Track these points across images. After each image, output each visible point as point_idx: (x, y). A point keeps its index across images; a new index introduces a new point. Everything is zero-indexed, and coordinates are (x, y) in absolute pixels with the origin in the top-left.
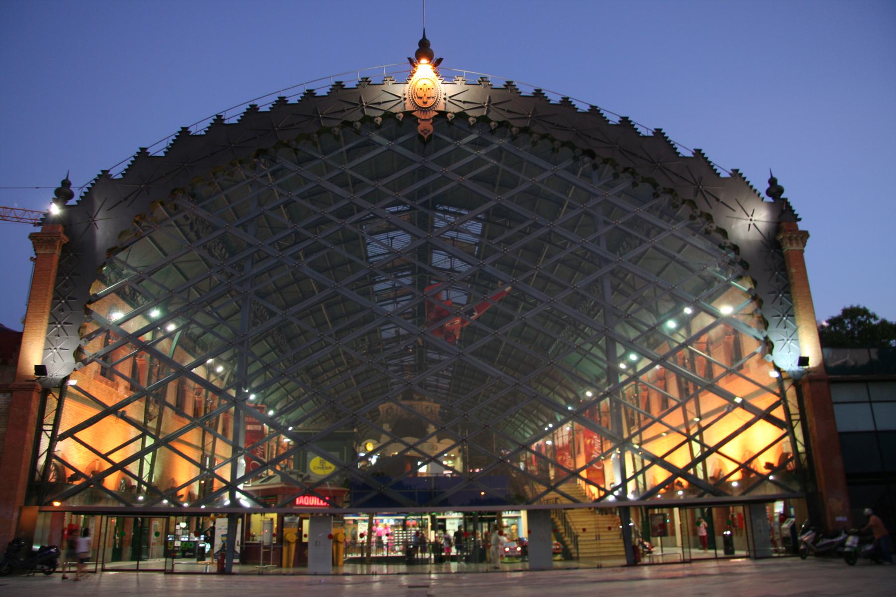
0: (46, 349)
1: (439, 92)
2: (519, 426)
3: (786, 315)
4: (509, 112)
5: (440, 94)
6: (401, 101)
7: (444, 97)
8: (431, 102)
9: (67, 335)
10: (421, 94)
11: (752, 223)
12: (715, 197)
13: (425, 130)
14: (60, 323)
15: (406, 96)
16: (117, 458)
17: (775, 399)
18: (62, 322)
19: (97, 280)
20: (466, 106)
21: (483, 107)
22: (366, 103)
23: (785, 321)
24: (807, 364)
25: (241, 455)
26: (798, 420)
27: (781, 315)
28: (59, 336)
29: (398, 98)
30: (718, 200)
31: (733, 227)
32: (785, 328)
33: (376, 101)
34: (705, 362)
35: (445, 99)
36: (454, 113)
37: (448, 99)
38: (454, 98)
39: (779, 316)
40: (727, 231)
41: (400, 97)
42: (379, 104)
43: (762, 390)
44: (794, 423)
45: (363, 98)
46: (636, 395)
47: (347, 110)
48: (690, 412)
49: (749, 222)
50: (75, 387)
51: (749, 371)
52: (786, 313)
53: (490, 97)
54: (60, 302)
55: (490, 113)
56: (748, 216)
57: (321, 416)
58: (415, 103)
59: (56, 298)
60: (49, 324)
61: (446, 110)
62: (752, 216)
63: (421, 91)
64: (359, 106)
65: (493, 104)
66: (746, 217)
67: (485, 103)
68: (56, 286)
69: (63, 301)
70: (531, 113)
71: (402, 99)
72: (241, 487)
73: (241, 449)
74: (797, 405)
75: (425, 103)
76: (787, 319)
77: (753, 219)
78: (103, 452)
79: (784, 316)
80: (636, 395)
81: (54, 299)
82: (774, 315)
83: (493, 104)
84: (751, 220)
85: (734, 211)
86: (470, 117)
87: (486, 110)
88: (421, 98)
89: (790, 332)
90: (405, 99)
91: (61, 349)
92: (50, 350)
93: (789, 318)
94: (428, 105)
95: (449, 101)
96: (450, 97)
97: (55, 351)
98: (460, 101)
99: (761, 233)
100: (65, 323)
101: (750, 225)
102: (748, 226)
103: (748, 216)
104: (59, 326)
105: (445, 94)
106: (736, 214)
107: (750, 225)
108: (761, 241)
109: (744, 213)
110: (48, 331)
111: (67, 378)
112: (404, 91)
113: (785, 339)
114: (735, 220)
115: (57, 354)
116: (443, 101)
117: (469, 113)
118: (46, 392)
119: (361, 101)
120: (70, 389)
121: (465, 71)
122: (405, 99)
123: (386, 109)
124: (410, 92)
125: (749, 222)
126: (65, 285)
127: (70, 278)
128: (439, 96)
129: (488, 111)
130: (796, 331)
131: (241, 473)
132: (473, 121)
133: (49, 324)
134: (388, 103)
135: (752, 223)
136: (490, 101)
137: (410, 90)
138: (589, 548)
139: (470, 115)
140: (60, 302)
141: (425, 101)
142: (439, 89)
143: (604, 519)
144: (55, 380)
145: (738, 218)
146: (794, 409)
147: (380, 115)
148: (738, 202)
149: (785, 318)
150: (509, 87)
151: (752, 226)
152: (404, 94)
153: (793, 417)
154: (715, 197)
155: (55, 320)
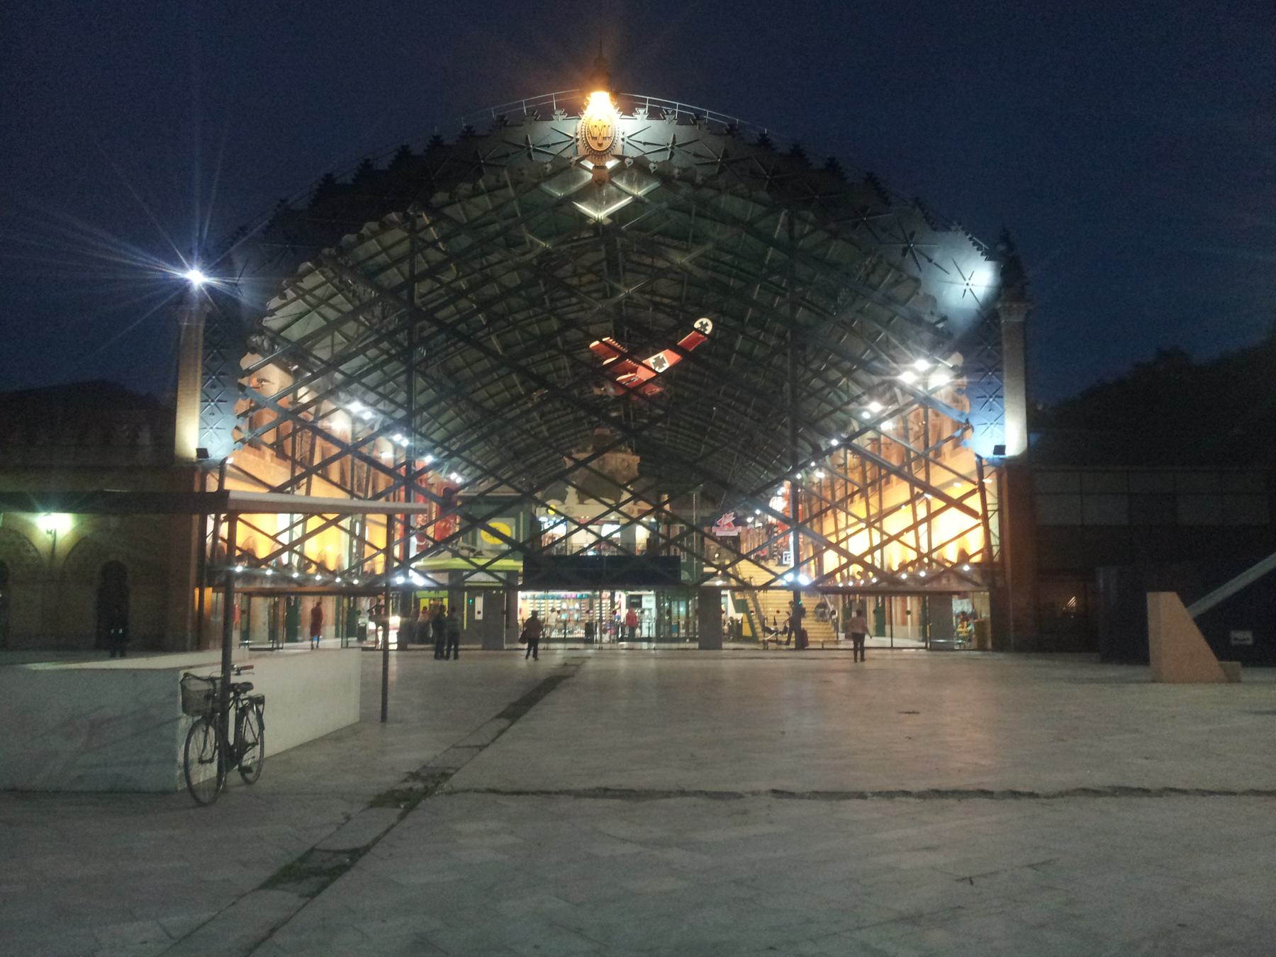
0: (202, 428)
1: (617, 130)
2: (775, 458)
3: (994, 396)
4: (696, 155)
5: (617, 133)
6: (573, 143)
7: (622, 137)
8: (606, 144)
9: (223, 414)
10: (596, 133)
11: (968, 288)
12: (927, 258)
13: (600, 180)
14: (213, 401)
15: (578, 137)
16: (284, 539)
17: (970, 487)
18: (216, 400)
19: (249, 353)
20: (647, 149)
21: (666, 149)
22: (533, 145)
23: (991, 403)
24: (1003, 453)
25: (412, 535)
26: (995, 511)
27: (988, 396)
28: (213, 414)
29: (570, 139)
30: (930, 261)
31: (944, 293)
32: (990, 410)
33: (545, 143)
34: (904, 449)
35: (623, 140)
36: (632, 158)
37: (626, 140)
38: (633, 138)
39: (985, 397)
40: (936, 297)
41: (572, 138)
42: (548, 146)
43: (960, 479)
44: (990, 514)
45: (529, 138)
46: (924, 423)
47: (513, 153)
48: (872, 506)
49: (965, 287)
50: (233, 465)
51: (945, 459)
52: (993, 394)
53: (674, 135)
54: (211, 378)
55: (674, 158)
56: (965, 279)
57: (502, 391)
58: (589, 145)
59: (208, 371)
60: (202, 401)
61: (625, 155)
62: (970, 279)
63: (595, 129)
64: (525, 149)
65: (678, 146)
66: (963, 280)
67: (668, 144)
68: (204, 360)
69: (214, 377)
70: (721, 156)
71: (574, 140)
72: (413, 565)
73: (414, 529)
74: (996, 496)
75: (600, 145)
76: (994, 400)
77: (970, 284)
78: (272, 534)
79: (991, 397)
80: (924, 423)
81: (203, 374)
82: (978, 395)
83: (677, 146)
84: (967, 284)
85: (948, 273)
86: (651, 162)
87: (669, 153)
88: (596, 138)
89: (994, 414)
90: (577, 140)
91: (218, 428)
92: (206, 430)
93: (997, 399)
94: (604, 148)
95: (628, 143)
96: (629, 137)
97: (211, 430)
98: (640, 142)
99: (977, 300)
100: (219, 401)
101: (965, 291)
102: (963, 292)
103: (965, 279)
104: (212, 404)
105: (623, 133)
106: (949, 278)
107: (965, 291)
108: (977, 311)
109: (961, 277)
110: (203, 409)
111: (225, 459)
112: (576, 129)
113: (989, 423)
114: (948, 284)
115: (213, 434)
116: (621, 142)
117: (651, 158)
118: (206, 471)
119: (527, 143)
120: (228, 468)
121: (648, 98)
122: (577, 140)
123: (556, 153)
124: (583, 130)
125: (965, 287)
126: (214, 359)
127: (219, 352)
128: (617, 136)
129: (672, 154)
130: (1002, 414)
131: (413, 553)
132: (654, 168)
133: (202, 401)
134: (558, 145)
135: (968, 288)
136: (674, 142)
137: (583, 127)
138: (816, 633)
139: (651, 160)
140: (211, 378)
141: (600, 142)
142: (616, 127)
143: (811, 602)
144: (214, 461)
145: (951, 282)
146: (991, 499)
147: (549, 160)
148: (955, 263)
149: (991, 400)
150: (698, 122)
151: (968, 293)
152: (577, 134)
153: (989, 508)
154: (927, 258)
155: (207, 398)
